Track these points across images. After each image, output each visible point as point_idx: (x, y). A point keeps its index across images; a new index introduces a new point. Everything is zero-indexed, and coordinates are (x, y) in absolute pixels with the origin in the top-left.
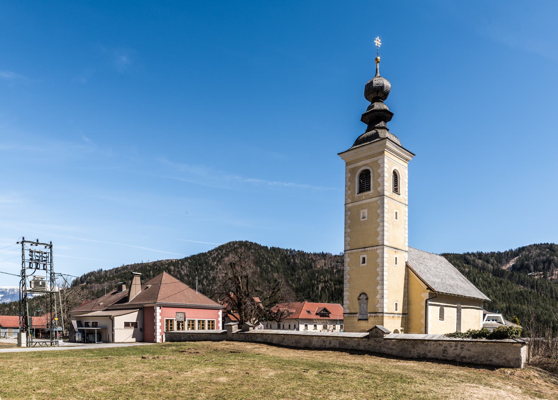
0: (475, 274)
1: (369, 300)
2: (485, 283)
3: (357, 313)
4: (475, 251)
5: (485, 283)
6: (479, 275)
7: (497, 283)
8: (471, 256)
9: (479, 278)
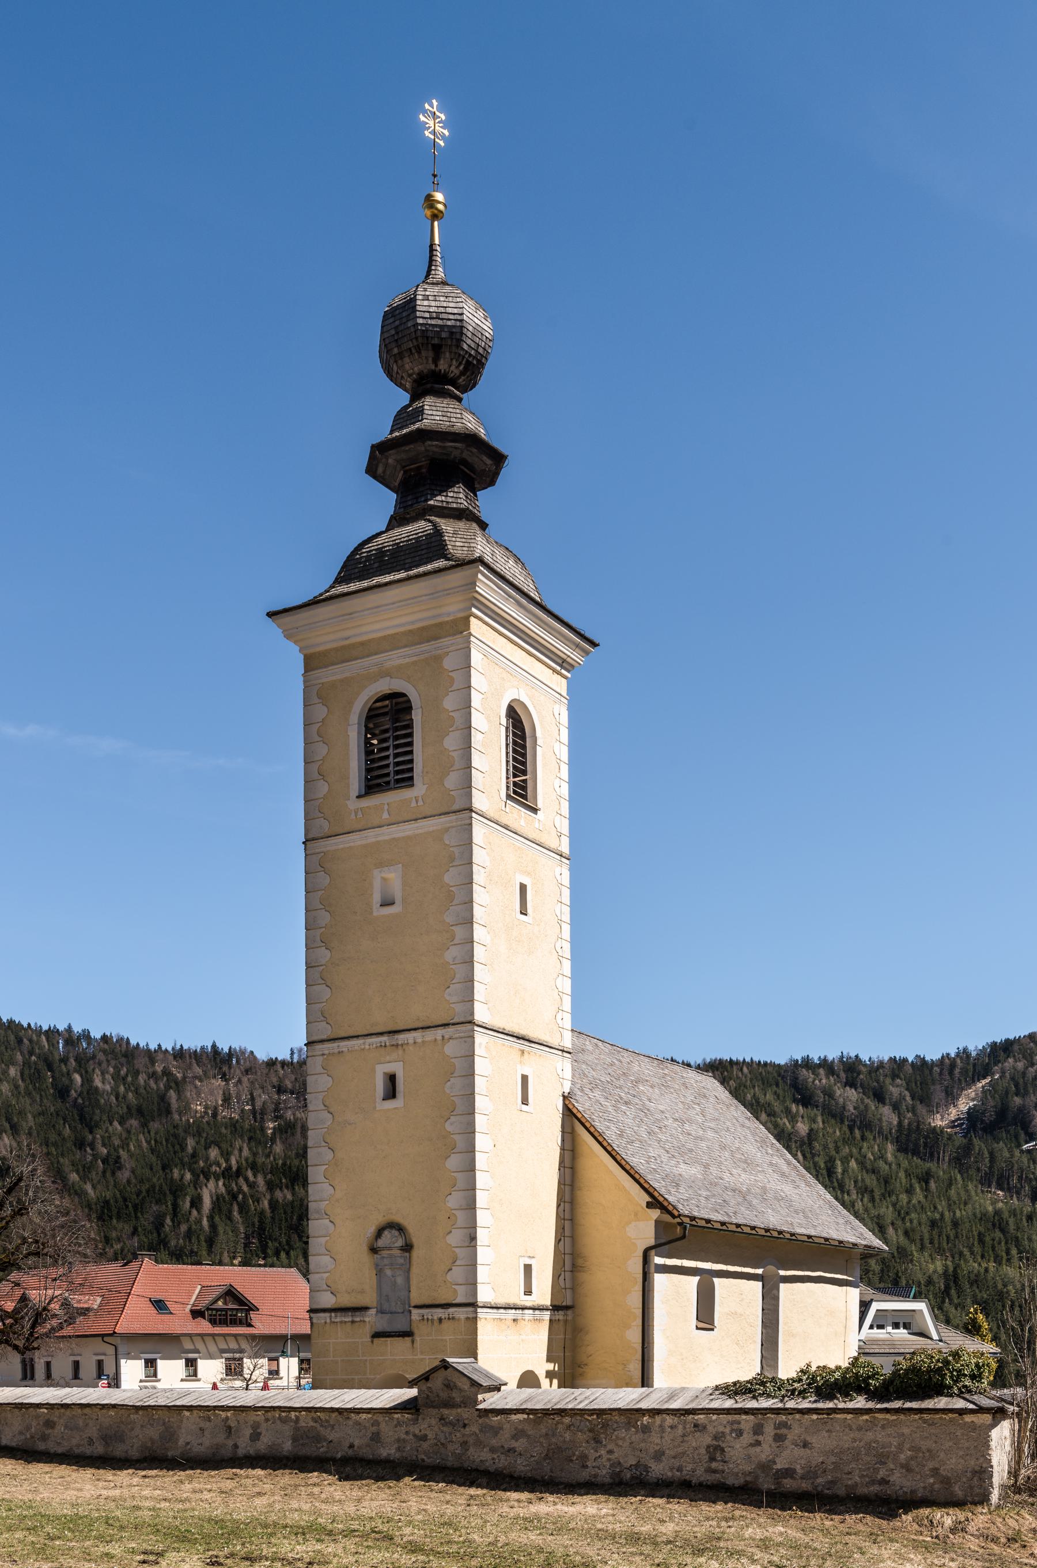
0: (831, 1146)
1: (415, 1253)
2: (871, 1181)
3: (366, 1309)
5: (871, 1181)
6: (847, 1150)
8: (817, 1075)
9: (845, 1161)
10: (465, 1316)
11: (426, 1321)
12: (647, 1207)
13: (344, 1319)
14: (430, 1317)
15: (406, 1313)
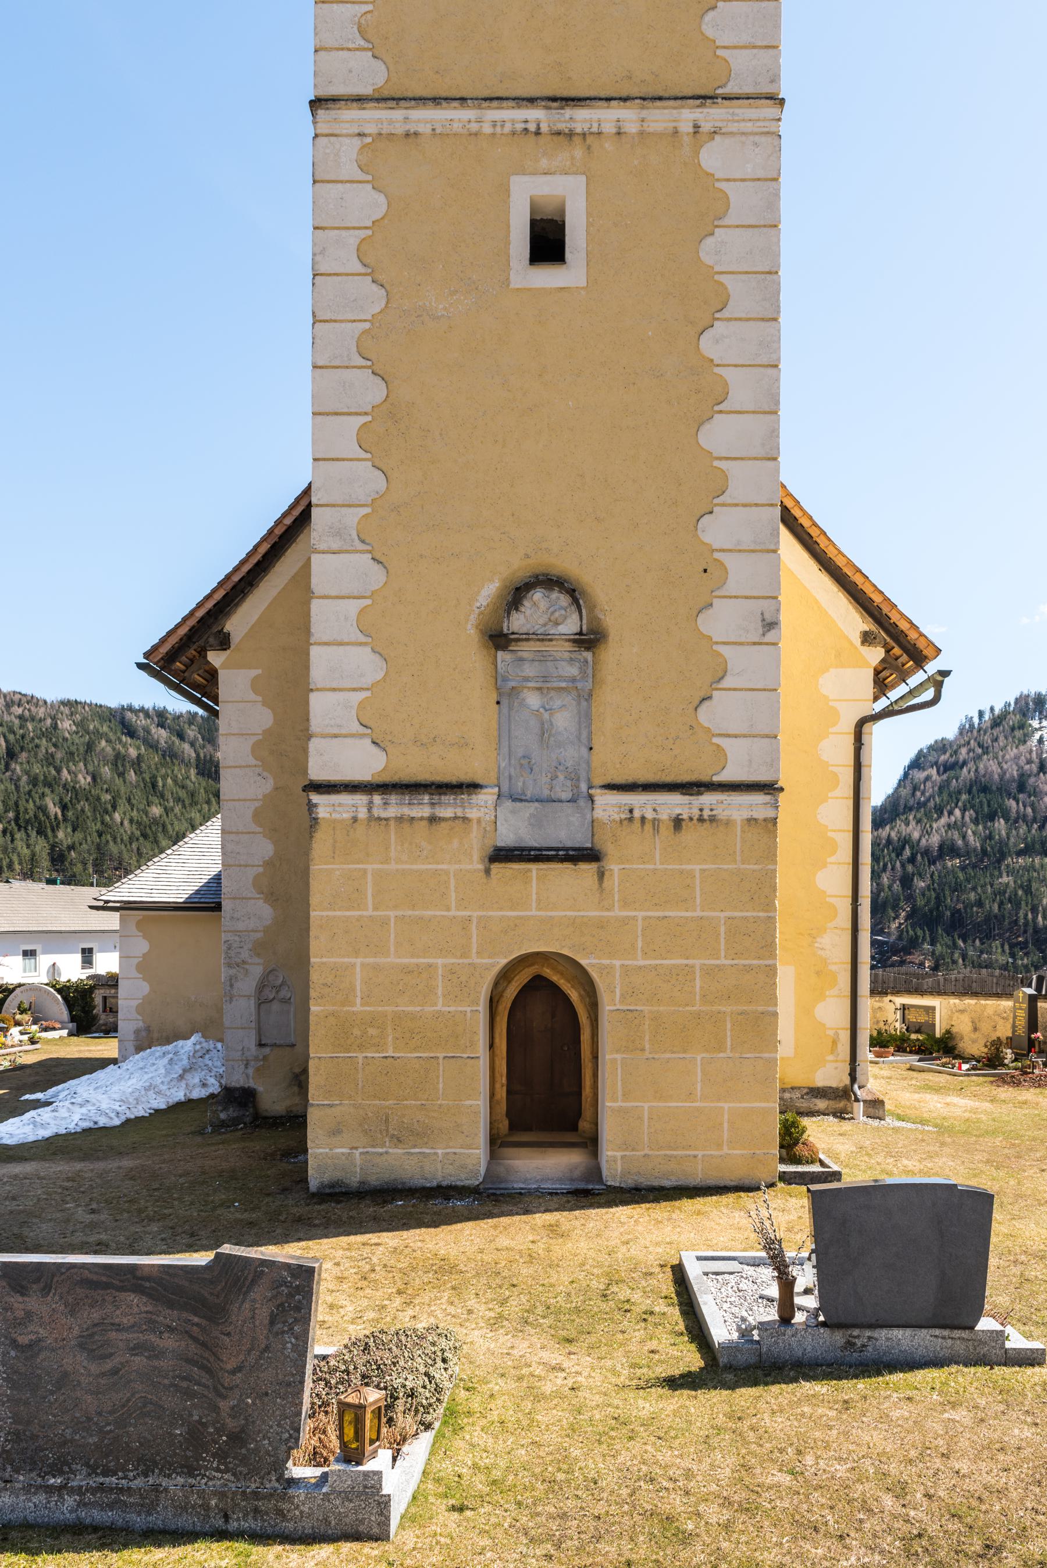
0: (153, 767)
1: (611, 654)
2: (182, 794)
3: (474, 787)
4: (148, 705)
5: (182, 794)
6: (164, 771)
7: (211, 796)
8: (138, 717)
9: (164, 778)
10: (746, 814)
11: (637, 824)
12: (863, 643)
13: (407, 811)
14: (650, 815)
15: (582, 803)
